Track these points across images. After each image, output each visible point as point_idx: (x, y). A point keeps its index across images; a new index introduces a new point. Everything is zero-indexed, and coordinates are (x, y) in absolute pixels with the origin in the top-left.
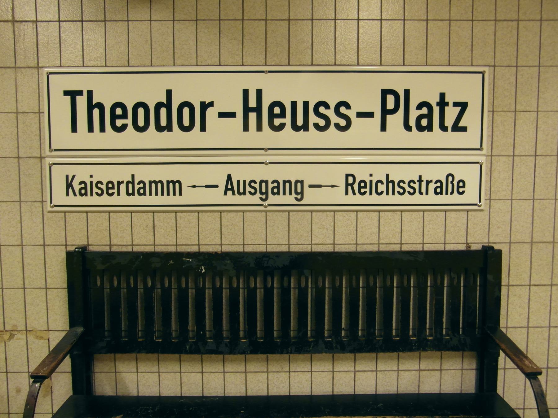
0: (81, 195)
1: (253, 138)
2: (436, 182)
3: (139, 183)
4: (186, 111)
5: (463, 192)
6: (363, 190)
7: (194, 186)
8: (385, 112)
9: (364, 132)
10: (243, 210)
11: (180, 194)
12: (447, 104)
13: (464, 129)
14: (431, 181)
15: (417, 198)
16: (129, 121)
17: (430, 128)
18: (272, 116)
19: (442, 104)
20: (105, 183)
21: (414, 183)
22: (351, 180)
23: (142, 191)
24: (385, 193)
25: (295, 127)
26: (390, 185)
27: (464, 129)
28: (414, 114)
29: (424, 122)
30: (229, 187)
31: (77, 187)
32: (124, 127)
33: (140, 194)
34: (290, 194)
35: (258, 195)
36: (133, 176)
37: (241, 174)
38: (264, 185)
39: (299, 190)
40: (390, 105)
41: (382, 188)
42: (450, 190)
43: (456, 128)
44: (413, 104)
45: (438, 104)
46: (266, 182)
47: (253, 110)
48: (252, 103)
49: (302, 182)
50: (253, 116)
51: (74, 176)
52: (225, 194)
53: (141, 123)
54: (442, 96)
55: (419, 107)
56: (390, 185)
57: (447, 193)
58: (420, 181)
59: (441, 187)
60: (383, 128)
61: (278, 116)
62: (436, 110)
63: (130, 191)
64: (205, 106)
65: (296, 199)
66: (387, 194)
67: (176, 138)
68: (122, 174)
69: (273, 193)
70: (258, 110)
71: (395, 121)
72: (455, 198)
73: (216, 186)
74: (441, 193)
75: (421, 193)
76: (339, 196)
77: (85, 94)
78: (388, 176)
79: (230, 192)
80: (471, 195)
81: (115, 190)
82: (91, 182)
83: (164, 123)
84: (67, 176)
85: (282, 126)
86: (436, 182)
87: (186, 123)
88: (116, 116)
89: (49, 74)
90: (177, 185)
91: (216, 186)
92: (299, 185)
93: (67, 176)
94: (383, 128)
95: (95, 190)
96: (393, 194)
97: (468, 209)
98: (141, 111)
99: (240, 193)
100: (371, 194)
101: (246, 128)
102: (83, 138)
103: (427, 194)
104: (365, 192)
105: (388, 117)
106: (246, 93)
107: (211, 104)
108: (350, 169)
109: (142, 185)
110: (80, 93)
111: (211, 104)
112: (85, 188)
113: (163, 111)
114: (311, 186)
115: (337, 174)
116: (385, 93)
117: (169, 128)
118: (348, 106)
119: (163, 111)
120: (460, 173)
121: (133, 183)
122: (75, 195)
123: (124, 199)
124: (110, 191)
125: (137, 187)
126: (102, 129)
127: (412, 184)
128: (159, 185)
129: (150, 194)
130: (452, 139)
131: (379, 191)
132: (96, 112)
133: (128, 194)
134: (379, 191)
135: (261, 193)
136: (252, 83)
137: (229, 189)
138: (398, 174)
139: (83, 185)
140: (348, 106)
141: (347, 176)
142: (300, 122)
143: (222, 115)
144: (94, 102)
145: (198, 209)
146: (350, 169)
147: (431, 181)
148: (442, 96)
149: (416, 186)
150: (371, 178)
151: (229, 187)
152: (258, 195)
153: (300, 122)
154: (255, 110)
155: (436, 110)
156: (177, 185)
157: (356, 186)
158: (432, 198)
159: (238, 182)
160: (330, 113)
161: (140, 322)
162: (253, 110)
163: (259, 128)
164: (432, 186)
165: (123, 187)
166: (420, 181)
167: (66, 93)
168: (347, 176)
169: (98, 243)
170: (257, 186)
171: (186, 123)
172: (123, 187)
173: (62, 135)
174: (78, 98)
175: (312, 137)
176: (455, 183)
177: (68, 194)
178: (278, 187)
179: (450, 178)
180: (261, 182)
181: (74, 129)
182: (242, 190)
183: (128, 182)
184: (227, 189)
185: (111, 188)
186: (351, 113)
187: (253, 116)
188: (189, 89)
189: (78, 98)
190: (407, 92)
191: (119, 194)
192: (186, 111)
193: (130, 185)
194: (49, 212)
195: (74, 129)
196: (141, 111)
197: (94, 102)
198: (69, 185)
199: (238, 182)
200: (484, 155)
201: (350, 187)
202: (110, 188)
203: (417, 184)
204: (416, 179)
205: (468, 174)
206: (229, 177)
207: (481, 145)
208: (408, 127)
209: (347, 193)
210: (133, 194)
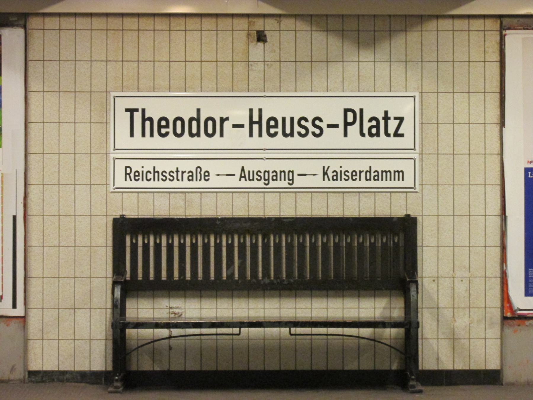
0: (333, 180)
1: (256, 142)
2: (189, 172)
3: (374, 172)
4: (210, 123)
5: (208, 180)
6: (137, 178)
7: (219, 175)
8: (347, 124)
9: (332, 138)
10: (255, 190)
11: (403, 180)
12: (389, 118)
13: (402, 135)
14: (185, 172)
15: (175, 184)
16: (170, 130)
17: (378, 134)
18: (269, 127)
19: (386, 118)
20: (350, 172)
21: (173, 172)
22: (128, 171)
23: (275, 178)
24: (152, 180)
25: (285, 135)
26: (156, 174)
27: (402, 135)
28: (367, 125)
29: (374, 131)
30: (243, 175)
31: (330, 174)
32: (167, 134)
33: (375, 180)
34: (285, 180)
35: (263, 181)
36: (370, 167)
37: (251, 166)
38: (266, 174)
39: (291, 178)
40: (350, 119)
41: (150, 176)
42: (199, 178)
43: (397, 134)
44: (366, 119)
45: (383, 118)
46: (268, 172)
47: (256, 123)
48: (256, 118)
49: (293, 172)
50: (256, 127)
51: (329, 167)
52: (240, 180)
53: (179, 131)
54: (386, 113)
55: (370, 120)
56: (156, 174)
57: (197, 180)
58: (177, 171)
59: (192, 176)
60: (346, 135)
61: (164, 127)
62: (382, 123)
63: (368, 178)
64: (223, 120)
65: (289, 184)
66: (154, 180)
67: (203, 141)
68: (362, 166)
69: (273, 180)
70: (260, 123)
71: (353, 130)
72: (203, 184)
73: (234, 175)
74: (192, 180)
75: (178, 180)
76: (318, 181)
77: (140, 111)
78: (154, 168)
79: (243, 179)
80: (408, 181)
81: (358, 177)
82: (341, 171)
83: (194, 131)
84: (324, 167)
85: (276, 134)
86: (188, 173)
87: (210, 131)
88: (162, 126)
89: (414, 97)
90: (401, 174)
91: (234, 175)
92: (291, 174)
93: (324, 167)
94: (346, 135)
95: (343, 176)
96: (158, 180)
97: (406, 191)
98: (179, 123)
99: (250, 180)
100: (143, 180)
101: (251, 135)
102: (138, 141)
103: (182, 180)
104: (356, 179)
105: (349, 128)
106: (251, 110)
107: (227, 119)
108: (326, 163)
109: (376, 174)
110: (137, 110)
111: (227, 119)
112: (337, 176)
113: (194, 123)
114: (299, 175)
115: (317, 167)
116: (346, 111)
117: (198, 135)
118: (321, 120)
119: (194, 123)
120: (205, 166)
121: (370, 172)
122: (329, 180)
123: (364, 183)
124: (354, 178)
125: (373, 175)
126: (152, 135)
127: (171, 174)
128: (388, 174)
129: (382, 180)
130: (394, 142)
131: (148, 178)
132: (148, 123)
133: (367, 180)
134: (148, 178)
135: (265, 180)
136: (256, 104)
137: (243, 177)
138: (161, 166)
139: (335, 174)
140: (321, 120)
141: (126, 167)
142: (288, 131)
143: (235, 126)
144: (146, 117)
145: (217, 191)
146: (326, 163)
147: (185, 172)
148: (386, 113)
149: (175, 175)
150: (143, 169)
151: (243, 175)
152: (263, 181)
153: (288, 131)
154: (257, 123)
155: (382, 123)
156: (401, 174)
157: (132, 175)
158: (186, 183)
159: (249, 172)
160: (309, 125)
161: (332, 272)
162: (256, 123)
163: (260, 135)
164: (186, 175)
165: (363, 175)
166: (177, 171)
167: (127, 110)
168: (126, 167)
169: (131, 213)
170: (262, 175)
171: (210, 131)
172: (363, 175)
173: (123, 139)
174: (135, 113)
175: (296, 141)
176: (202, 173)
177: (324, 180)
178: (276, 176)
179: (199, 170)
180: (265, 172)
181: (132, 135)
182: (251, 178)
183: (367, 172)
184: (241, 177)
185: (354, 176)
186: (323, 125)
187: (256, 127)
188: (211, 109)
189: (135, 113)
190: (361, 111)
191: (360, 180)
192: (210, 123)
193: (368, 174)
194: (112, 192)
195: (132, 135)
196: (179, 123)
197: (146, 117)
198: (325, 174)
199: (249, 172)
200: (417, 153)
201: (128, 176)
202: (354, 175)
203: (175, 173)
204: (175, 170)
205: (407, 167)
206: (243, 169)
207: (415, 147)
208: (363, 135)
209: (324, 180)
210: (370, 180)
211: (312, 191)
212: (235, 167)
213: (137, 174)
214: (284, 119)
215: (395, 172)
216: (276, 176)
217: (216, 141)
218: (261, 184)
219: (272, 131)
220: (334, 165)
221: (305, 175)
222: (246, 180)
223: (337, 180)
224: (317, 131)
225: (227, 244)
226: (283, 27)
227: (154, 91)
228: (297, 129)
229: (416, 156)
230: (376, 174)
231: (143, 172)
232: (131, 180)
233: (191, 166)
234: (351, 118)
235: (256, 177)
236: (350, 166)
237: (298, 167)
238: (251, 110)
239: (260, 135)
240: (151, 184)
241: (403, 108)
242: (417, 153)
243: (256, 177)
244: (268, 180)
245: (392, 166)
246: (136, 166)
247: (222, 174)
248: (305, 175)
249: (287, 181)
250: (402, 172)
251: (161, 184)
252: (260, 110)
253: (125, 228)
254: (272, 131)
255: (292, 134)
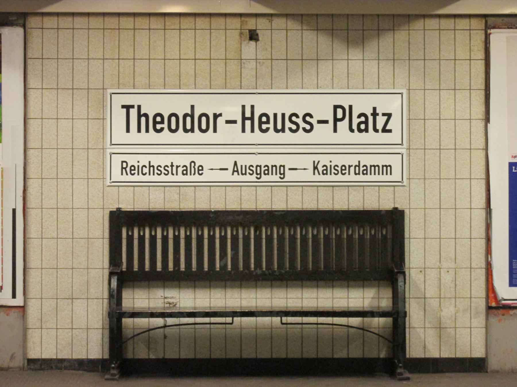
0: (323, 174)
1: (248, 137)
2: (183, 167)
3: (363, 167)
4: (204, 119)
5: (202, 174)
6: (133, 172)
7: (212, 169)
8: (336, 120)
9: (322, 133)
10: (248, 184)
11: (391, 174)
12: (378, 114)
13: (390, 131)
14: (180, 166)
15: (170, 178)
16: (165, 125)
17: (366, 130)
18: (261, 123)
19: (375, 114)
20: (340, 166)
21: (168, 167)
22: (125, 165)
23: (266, 172)
24: (148, 174)
25: (276, 130)
26: (152, 168)
27: (390, 131)
28: (356, 121)
29: (363, 127)
30: (236, 169)
31: (320, 169)
32: (162, 129)
33: (363, 174)
34: (276, 174)
35: (255, 175)
36: (359, 162)
37: (243, 161)
38: (258, 168)
39: (282, 172)
40: (340, 115)
41: (146, 170)
42: (193, 172)
43: (385, 130)
44: (355, 115)
45: (372, 114)
46: (260, 166)
47: (248, 119)
48: (248, 114)
49: (284, 166)
50: (248, 123)
51: (319, 162)
52: (233, 174)
53: (173, 127)
54: (375, 109)
55: (359, 116)
56: (152, 168)
57: (191, 174)
58: (172, 166)
59: (186, 170)
60: (335, 131)
61: (159, 123)
62: (371, 119)
63: (357, 172)
64: (216, 116)
65: (280, 178)
66: (150, 174)
67: (197, 136)
68: (352, 160)
69: (265, 174)
70: (252, 119)
71: (343, 126)
72: (197, 178)
73: (227, 169)
74: (187, 174)
75: (173, 174)
76: (309, 176)
77: (136, 107)
78: (150, 162)
79: (236, 173)
80: (396, 176)
81: (347, 171)
82: (331, 166)
83: (189, 127)
84: (314, 162)
85: (268, 129)
86: (183, 167)
87: (204, 127)
88: (157, 122)
89: (402, 94)
90: (389, 168)
91: (227, 169)
92: (282, 168)
93: (314, 162)
94: (335, 131)
95: (333, 171)
96: (154, 174)
97: (394, 185)
98: (173, 119)
99: (242, 174)
100: (138, 174)
101: (243, 131)
102: (134, 136)
103: (177, 174)
104: (345, 173)
105: (339, 123)
106: (243, 107)
107: (220, 115)
108: (316, 158)
109: (365, 168)
110: (133, 107)
111: (220, 115)
112: (326, 170)
113: (189, 119)
114: (290, 169)
115: (307, 162)
116: (336, 107)
117: (192, 130)
118: (311, 116)
119: (189, 119)
120: (199, 160)
121: (359, 166)
122: (319, 174)
123: (353, 177)
124: (343, 172)
125: (362, 169)
126: (147, 131)
127: (166, 168)
128: (377, 168)
129: (371, 174)
130: (382, 138)
131: (144, 173)
132: (143, 119)
133: (356, 174)
134: (144, 173)
135: (257, 174)
136: (248, 101)
137: (236, 171)
138: (156, 161)
139: (325, 168)
140: (311, 116)
141: (123, 162)
142: (279, 127)
143: (228, 122)
144: (142, 113)
145: (211, 185)
146: (316, 158)
147: (180, 166)
148: (375, 109)
149: (169, 169)
150: (138, 164)
151: (236, 169)
152: (255, 175)
153: (279, 127)
154: (249, 119)
155: (371, 119)
156: (389, 168)
157: (128, 169)
158: (180, 178)
159: (242, 166)
160: (300, 121)
162: (248, 119)
163: (252, 131)
164: (180, 170)
165: (352, 169)
166: (172, 166)
167: (123, 107)
168: (123, 162)
169: (127, 206)
170: (254, 169)
171: (204, 127)
172: (352, 169)
173: (119, 134)
174: (131, 110)
175: (287, 137)
176: (196, 167)
177: (314, 174)
178: (268, 170)
179: (193, 164)
180: (257, 166)
181: (128, 131)
182: (244, 172)
183: (356, 166)
184: (234, 171)
185: (344, 170)
186: (314, 121)
187: (248, 123)
188: (205, 105)
189: (131, 110)
190: (351, 107)
191: (349, 174)
192: (204, 119)
193: (357, 168)
194: (109, 186)
195: (128, 131)
196: (173, 119)
197: (142, 113)
198: (315, 168)
199: (242, 166)
200: (404, 148)
201: (124, 170)
202: (343, 169)
203: (170, 168)
204: (169, 165)
205: (394, 161)
206: (236, 163)
207: (402, 142)
208: (352, 130)
209: (314, 174)
210: (359, 174)
211: (302, 185)
212: (228, 162)
213: (133, 168)
214: (275, 115)
215: (383, 166)
216: (268, 170)
217: (210, 137)
218: (253, 178)
219: (264, 127)
220: (324, 160)
221: (296, 169)
222: (238, 174)
223: (327, 174)
224: (308, 127)
225: (221, 236)
226: (274, 26)
227: (150, 88)
228: (288, 124)
229: (404, 151)
230: (365, 168)
231: (138, 166)
232: (127, 174)
233: (186, 160)
234: (341, 114)
235: (248, 171)
236: (339, 161)
237: (289, 161)
238: (243, 107)
239: (252, 131)
240: (147, 178)
241: (391, 104)
242: (404, 148)
243: (248, 171)
244: (260, 174)
245: (380, 160)
246: (132, 160)
247: (216, 168)
248: (296, 169)
249: (278, 175)
250: (390, 166)
251: (156, 178)
252: (252, 107)
253: (121, 221)
254: (264, 127)
255: (283, 130)
